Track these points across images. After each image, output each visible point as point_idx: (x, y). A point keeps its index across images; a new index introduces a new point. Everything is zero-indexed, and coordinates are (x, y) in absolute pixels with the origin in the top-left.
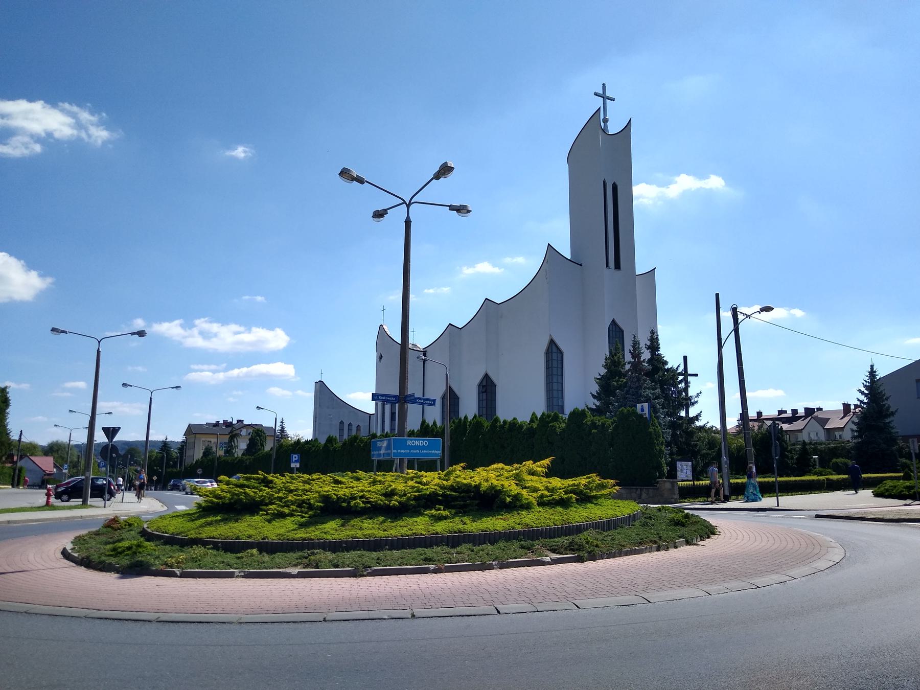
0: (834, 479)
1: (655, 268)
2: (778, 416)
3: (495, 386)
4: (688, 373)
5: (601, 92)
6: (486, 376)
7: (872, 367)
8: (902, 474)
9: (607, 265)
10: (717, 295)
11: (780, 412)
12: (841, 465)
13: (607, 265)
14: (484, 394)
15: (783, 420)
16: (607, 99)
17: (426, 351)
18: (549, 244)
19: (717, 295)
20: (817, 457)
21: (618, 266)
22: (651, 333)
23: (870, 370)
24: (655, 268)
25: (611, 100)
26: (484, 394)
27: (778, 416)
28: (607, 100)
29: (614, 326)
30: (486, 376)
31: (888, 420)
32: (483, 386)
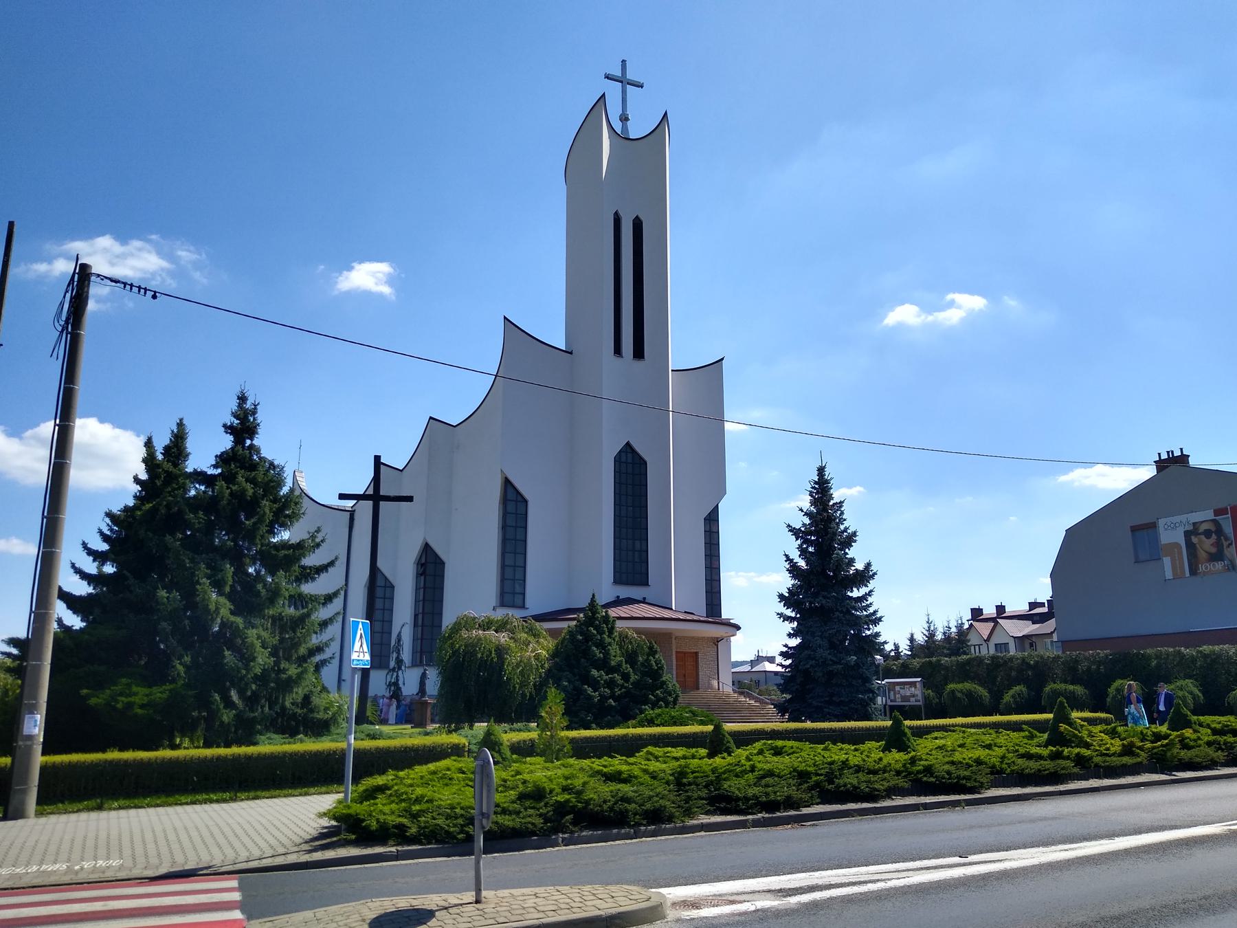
0: (766, 729)
1: (722, 359)
2: (1030, 610)
3: (443, 563)
4: (381, 494)
5: (618, 73)
6: (427, 548)
7: (821, 470)
8: (1051, 716)
9: (618, 351)
10: (11, 225)
11: (1033, 605)
12: (959, 695)
13: (618, 351)
14: (422, 578)
15: (1035, 618)
16: (628, 84)
17: (354, 511)
18: (505, 318)
19: (11, 225)
20: (919, 679)
21: (639, 353)
22: (239, 398)
23: (816, 479)
24: (722, 359)
25: (638, 86)
26: (422, 578)
27: (1030, 610)
28: (628, 86)
29: (630, 455)
30: (427, 548)
31: (856, 593)
32: (422, 565)
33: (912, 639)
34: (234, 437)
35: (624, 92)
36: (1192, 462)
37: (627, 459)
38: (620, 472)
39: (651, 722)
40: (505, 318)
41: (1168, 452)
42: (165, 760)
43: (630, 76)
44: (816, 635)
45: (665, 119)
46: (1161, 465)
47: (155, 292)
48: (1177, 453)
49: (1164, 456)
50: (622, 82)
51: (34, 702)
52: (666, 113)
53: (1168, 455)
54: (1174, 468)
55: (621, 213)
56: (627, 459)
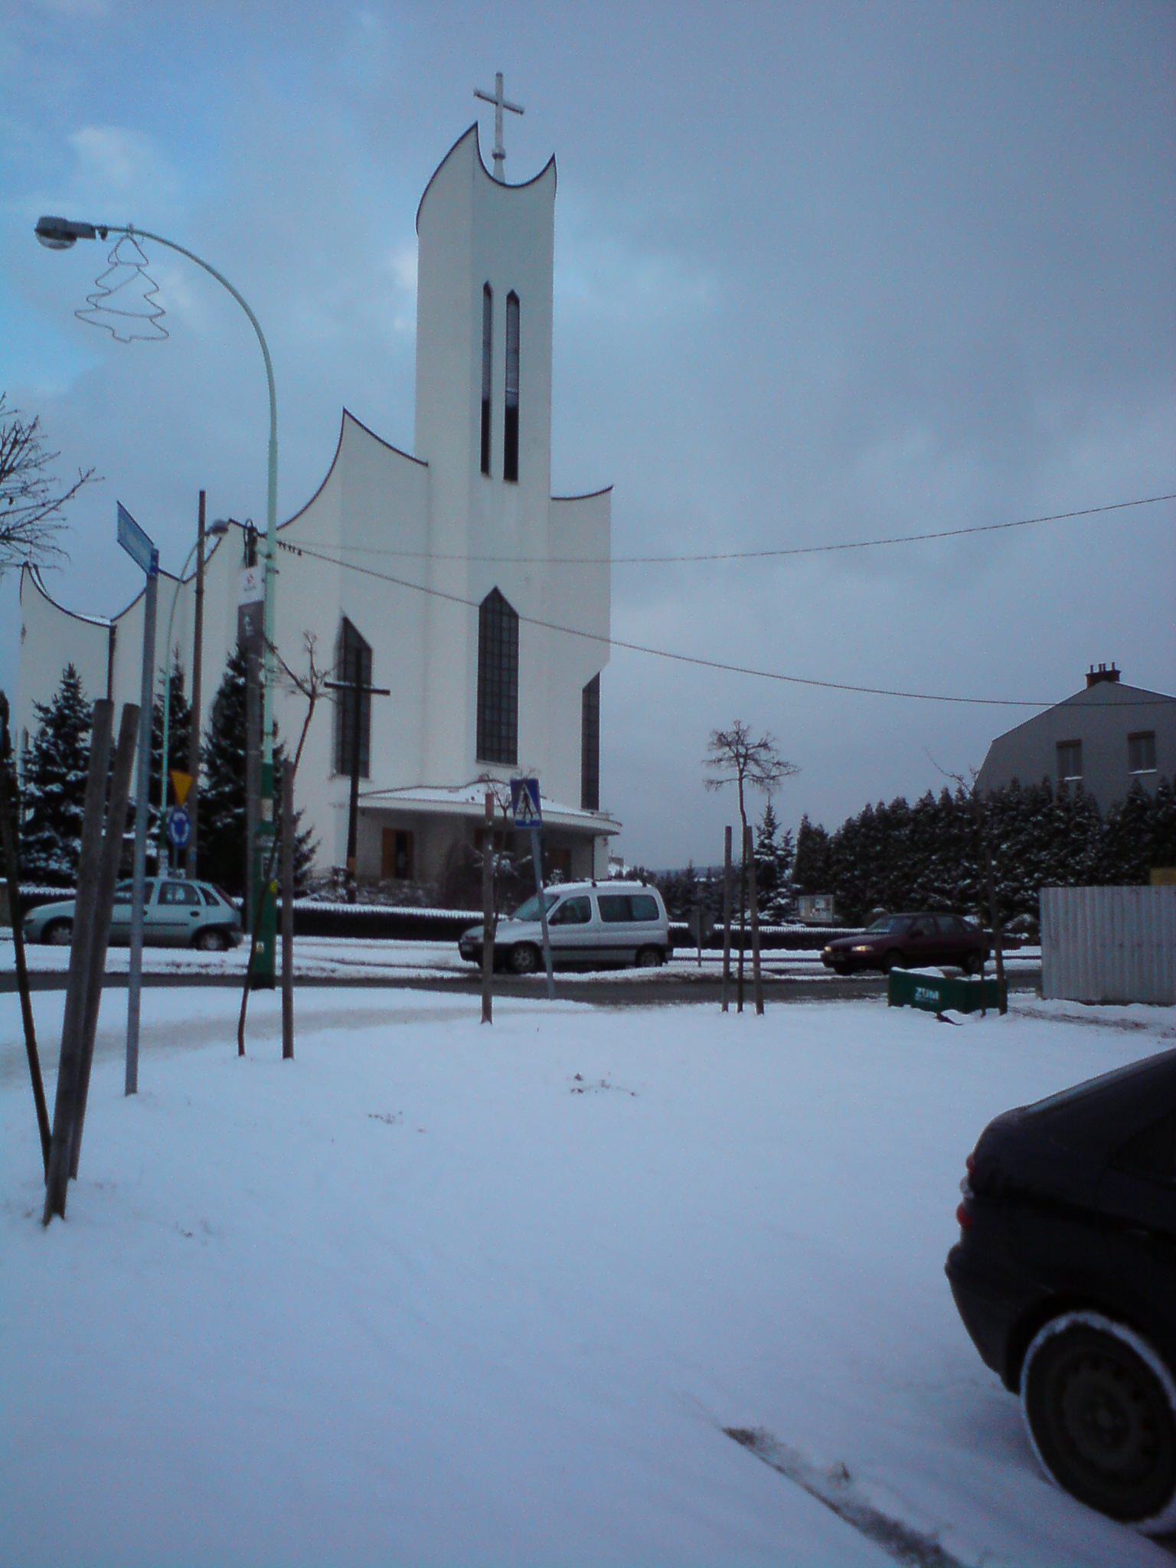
1: (610, 489)
9: (485, 467)
18: (345, 411)
21: (511, 473)
24: (610, 489)
33: (881, 804)
34: (908, 1003)
35: (499, 117)
36: (1123, 680)
37: (719, 960)
38: (501, 642)
39: (323, 899)
40: (345, 411)
41: (1100, 665)
42: (679, 872)
43: (509, 97)
44: (739, 747)
45: (550, 170)
46: (1093, 679)
47: (202, 533)
48: (1109, 668)
49: (1096, 670)
50: (497, 103)
51: (529, 857)
52: (553, 159)
53: (1100, 669)
54: (1103, 685)
55: (493, 286)
56: (719, 960)
